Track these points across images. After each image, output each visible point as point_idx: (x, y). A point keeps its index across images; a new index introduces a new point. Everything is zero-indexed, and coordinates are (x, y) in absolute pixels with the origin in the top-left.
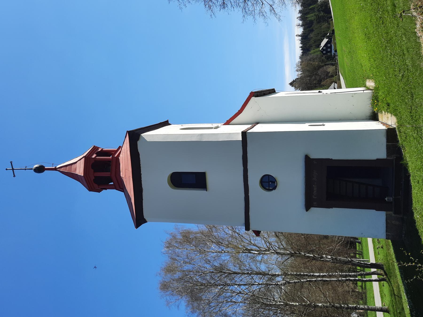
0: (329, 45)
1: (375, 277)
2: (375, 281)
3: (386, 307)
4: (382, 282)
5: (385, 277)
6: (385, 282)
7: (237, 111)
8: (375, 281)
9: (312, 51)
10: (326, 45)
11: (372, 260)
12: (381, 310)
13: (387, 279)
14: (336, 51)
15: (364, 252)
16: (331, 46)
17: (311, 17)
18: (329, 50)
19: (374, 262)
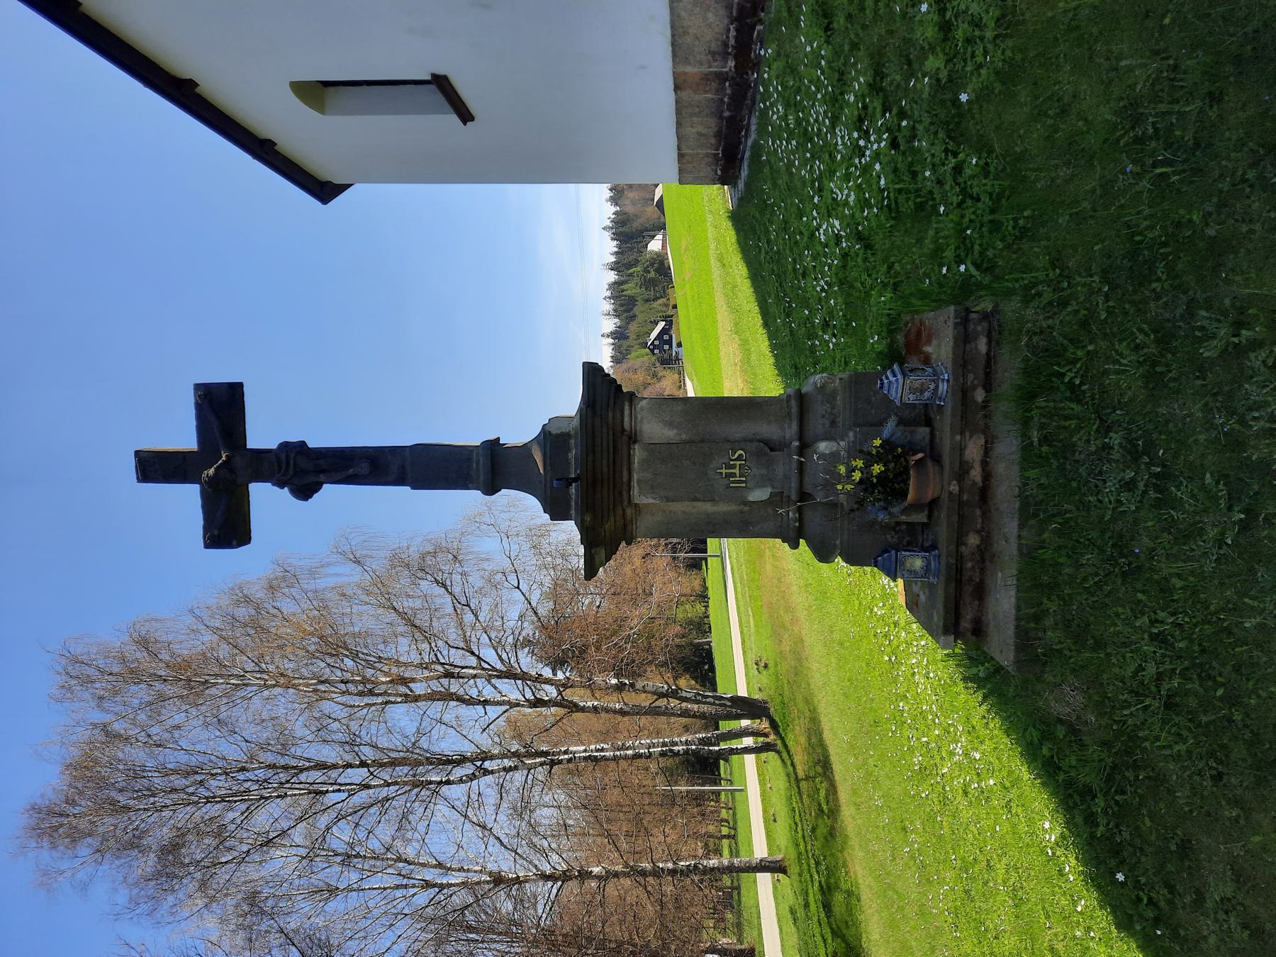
0: (666, 337)
1: (748, 741)
2: (747, 750)
3: (779, 857)
4: (764, 756)
5: (772, 737)
6: (771, 755)
7: (472, 437)
8: (747, 750)
9: (633, 354)
10: (659, 337)
11: (760, 851)
12: (763, 867)
13: (779, 742)
14: (679, 345)
15: (713, 620)
16: (671, 337)
17: (631, 289)
18: (666, 347)
19: (743, 692)
